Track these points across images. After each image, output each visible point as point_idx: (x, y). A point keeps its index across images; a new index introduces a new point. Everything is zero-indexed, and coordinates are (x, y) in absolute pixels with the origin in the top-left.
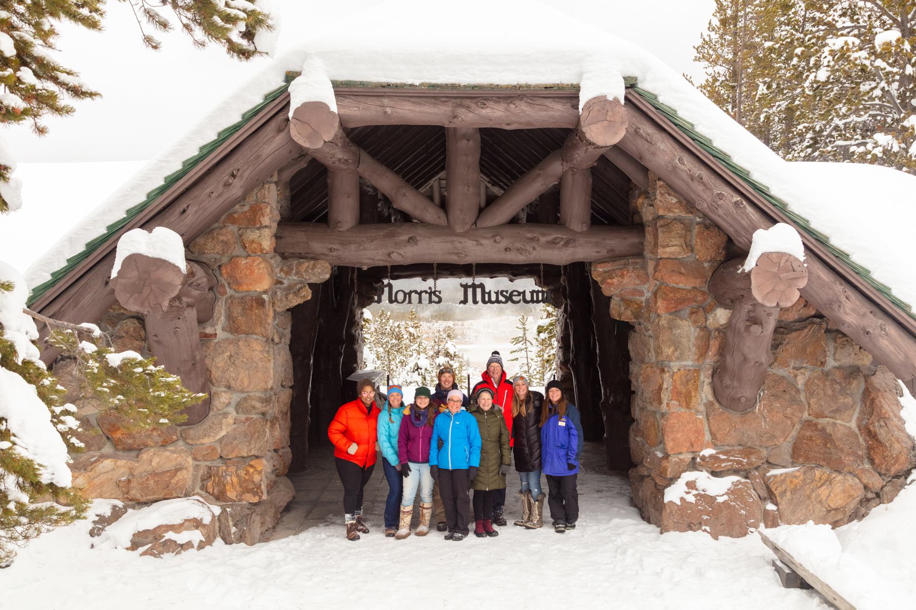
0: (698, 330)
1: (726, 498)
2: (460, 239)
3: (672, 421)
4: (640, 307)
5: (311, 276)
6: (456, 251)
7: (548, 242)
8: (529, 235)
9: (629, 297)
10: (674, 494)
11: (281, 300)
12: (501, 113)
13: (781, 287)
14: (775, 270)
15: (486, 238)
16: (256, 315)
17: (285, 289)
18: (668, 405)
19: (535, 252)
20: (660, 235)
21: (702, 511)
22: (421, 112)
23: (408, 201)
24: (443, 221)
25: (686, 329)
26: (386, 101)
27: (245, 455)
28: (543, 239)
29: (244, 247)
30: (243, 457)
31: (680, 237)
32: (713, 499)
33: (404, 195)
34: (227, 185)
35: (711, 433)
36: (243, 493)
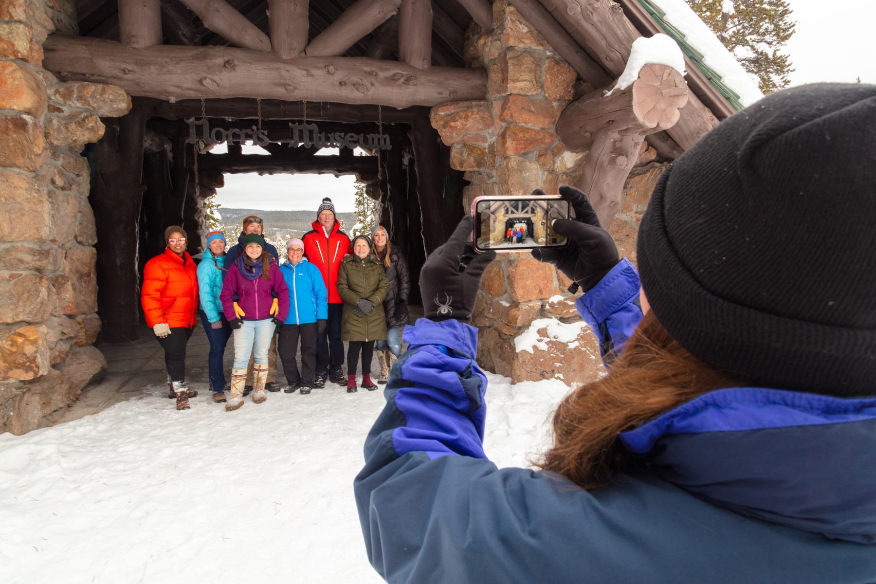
0: (546, 173)
1: (576, 344)
2: (288, 67)
3: (521, 268)
4: (483, 153)
5: (101, 104)
6: (282, 81)
7: (387, 78)
8: (367, 69)
9: (472, 142)
10: (525, 342)
11: (59, 130)
13: (662, 105)
14: (657, 84)
15: (318, 68)
16: (14, 140)
17: (64, 118)
19: (372, 90)
20: (511, 68)
21: (554, 358)
23: (223, 20)
24: (266, 44)
25: (535, 172)
27: (9, 321)
28: (382, 75)
30: (8, 324)
31: (530, 72)
32: (565, 345)
33: (217, 10)
35: (559, 280)
36: (10, 369)
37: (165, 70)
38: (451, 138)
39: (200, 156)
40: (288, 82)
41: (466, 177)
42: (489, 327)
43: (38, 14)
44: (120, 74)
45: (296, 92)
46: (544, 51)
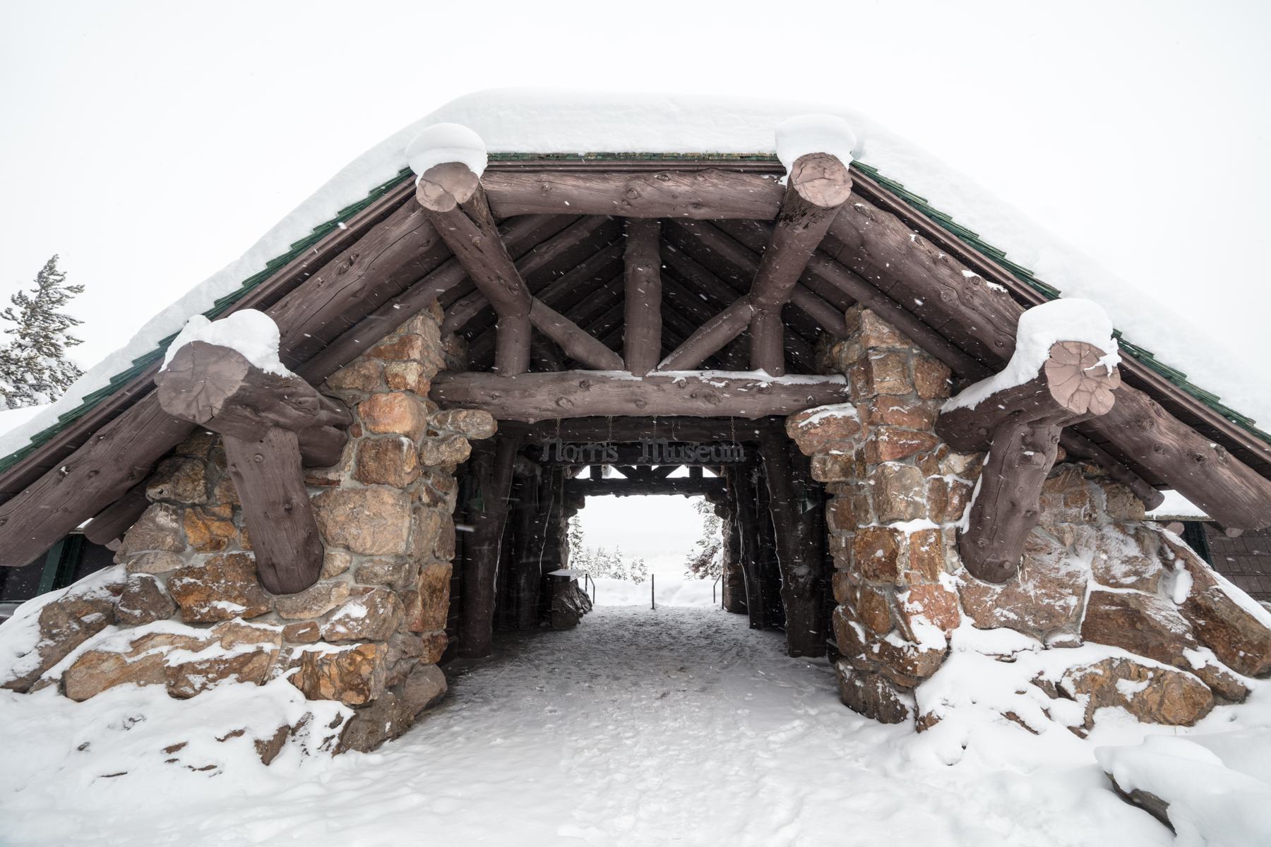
12: (687, 188)
18: (907, 575)
22: (588, 188)
23: (582, 344)
26: (544, 176)
29: (387, 382)
34: (342, 272)
36: (344, 690)
38: (811, 445)
39: (567, 481)
41: (829, 489)
42: (873, 672)
43: (432, 355)
44: (489, 399)
46: (910, 349)
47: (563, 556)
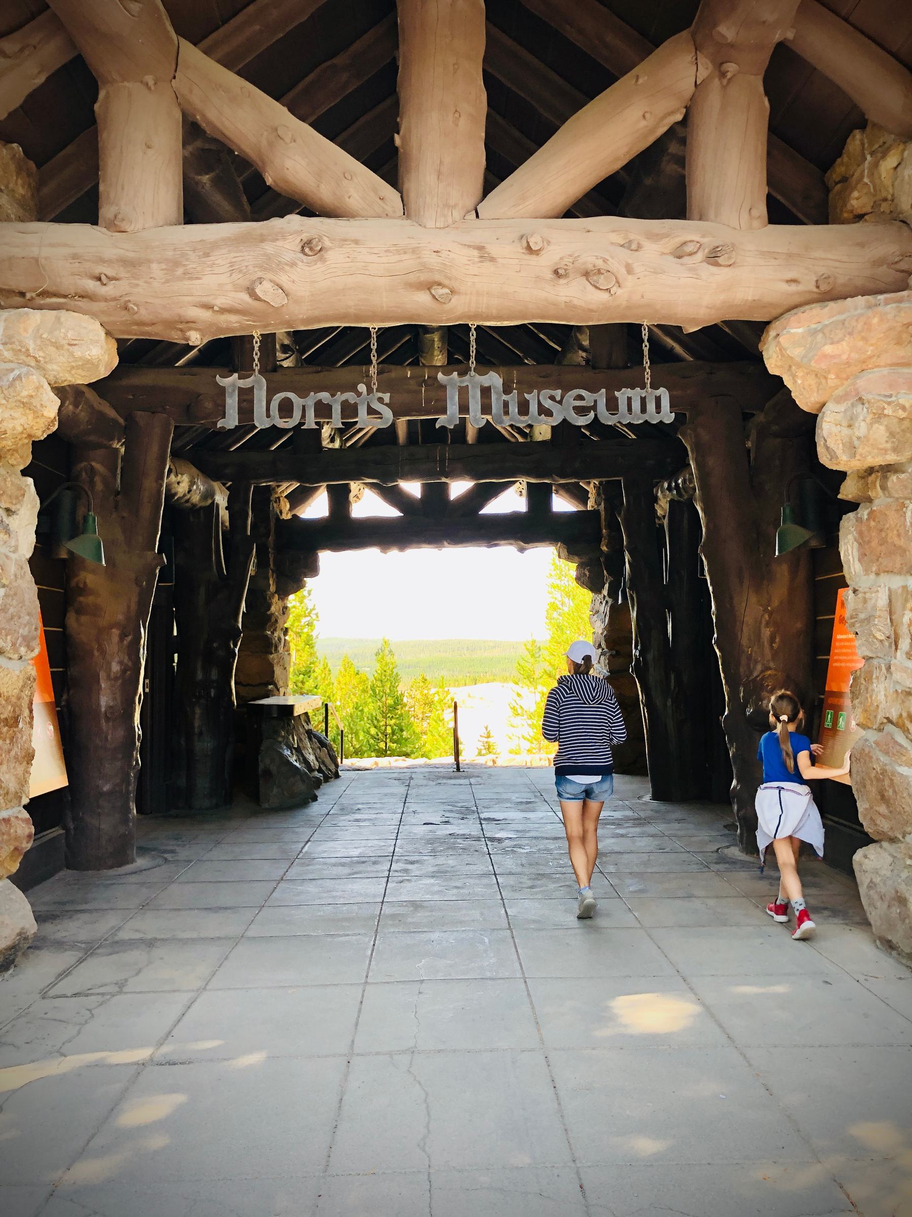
6: (424, 277)
23: (302, 154)
37: (180, 271)
40: (437, 277)
44: (91, 285)
45: (455, 300)
47: (278, 670)
